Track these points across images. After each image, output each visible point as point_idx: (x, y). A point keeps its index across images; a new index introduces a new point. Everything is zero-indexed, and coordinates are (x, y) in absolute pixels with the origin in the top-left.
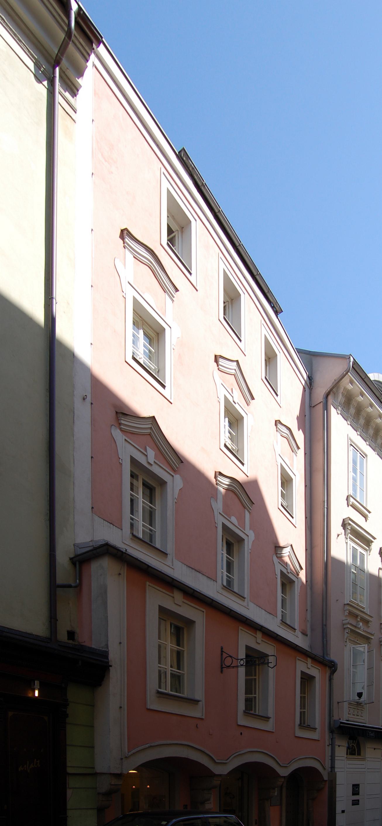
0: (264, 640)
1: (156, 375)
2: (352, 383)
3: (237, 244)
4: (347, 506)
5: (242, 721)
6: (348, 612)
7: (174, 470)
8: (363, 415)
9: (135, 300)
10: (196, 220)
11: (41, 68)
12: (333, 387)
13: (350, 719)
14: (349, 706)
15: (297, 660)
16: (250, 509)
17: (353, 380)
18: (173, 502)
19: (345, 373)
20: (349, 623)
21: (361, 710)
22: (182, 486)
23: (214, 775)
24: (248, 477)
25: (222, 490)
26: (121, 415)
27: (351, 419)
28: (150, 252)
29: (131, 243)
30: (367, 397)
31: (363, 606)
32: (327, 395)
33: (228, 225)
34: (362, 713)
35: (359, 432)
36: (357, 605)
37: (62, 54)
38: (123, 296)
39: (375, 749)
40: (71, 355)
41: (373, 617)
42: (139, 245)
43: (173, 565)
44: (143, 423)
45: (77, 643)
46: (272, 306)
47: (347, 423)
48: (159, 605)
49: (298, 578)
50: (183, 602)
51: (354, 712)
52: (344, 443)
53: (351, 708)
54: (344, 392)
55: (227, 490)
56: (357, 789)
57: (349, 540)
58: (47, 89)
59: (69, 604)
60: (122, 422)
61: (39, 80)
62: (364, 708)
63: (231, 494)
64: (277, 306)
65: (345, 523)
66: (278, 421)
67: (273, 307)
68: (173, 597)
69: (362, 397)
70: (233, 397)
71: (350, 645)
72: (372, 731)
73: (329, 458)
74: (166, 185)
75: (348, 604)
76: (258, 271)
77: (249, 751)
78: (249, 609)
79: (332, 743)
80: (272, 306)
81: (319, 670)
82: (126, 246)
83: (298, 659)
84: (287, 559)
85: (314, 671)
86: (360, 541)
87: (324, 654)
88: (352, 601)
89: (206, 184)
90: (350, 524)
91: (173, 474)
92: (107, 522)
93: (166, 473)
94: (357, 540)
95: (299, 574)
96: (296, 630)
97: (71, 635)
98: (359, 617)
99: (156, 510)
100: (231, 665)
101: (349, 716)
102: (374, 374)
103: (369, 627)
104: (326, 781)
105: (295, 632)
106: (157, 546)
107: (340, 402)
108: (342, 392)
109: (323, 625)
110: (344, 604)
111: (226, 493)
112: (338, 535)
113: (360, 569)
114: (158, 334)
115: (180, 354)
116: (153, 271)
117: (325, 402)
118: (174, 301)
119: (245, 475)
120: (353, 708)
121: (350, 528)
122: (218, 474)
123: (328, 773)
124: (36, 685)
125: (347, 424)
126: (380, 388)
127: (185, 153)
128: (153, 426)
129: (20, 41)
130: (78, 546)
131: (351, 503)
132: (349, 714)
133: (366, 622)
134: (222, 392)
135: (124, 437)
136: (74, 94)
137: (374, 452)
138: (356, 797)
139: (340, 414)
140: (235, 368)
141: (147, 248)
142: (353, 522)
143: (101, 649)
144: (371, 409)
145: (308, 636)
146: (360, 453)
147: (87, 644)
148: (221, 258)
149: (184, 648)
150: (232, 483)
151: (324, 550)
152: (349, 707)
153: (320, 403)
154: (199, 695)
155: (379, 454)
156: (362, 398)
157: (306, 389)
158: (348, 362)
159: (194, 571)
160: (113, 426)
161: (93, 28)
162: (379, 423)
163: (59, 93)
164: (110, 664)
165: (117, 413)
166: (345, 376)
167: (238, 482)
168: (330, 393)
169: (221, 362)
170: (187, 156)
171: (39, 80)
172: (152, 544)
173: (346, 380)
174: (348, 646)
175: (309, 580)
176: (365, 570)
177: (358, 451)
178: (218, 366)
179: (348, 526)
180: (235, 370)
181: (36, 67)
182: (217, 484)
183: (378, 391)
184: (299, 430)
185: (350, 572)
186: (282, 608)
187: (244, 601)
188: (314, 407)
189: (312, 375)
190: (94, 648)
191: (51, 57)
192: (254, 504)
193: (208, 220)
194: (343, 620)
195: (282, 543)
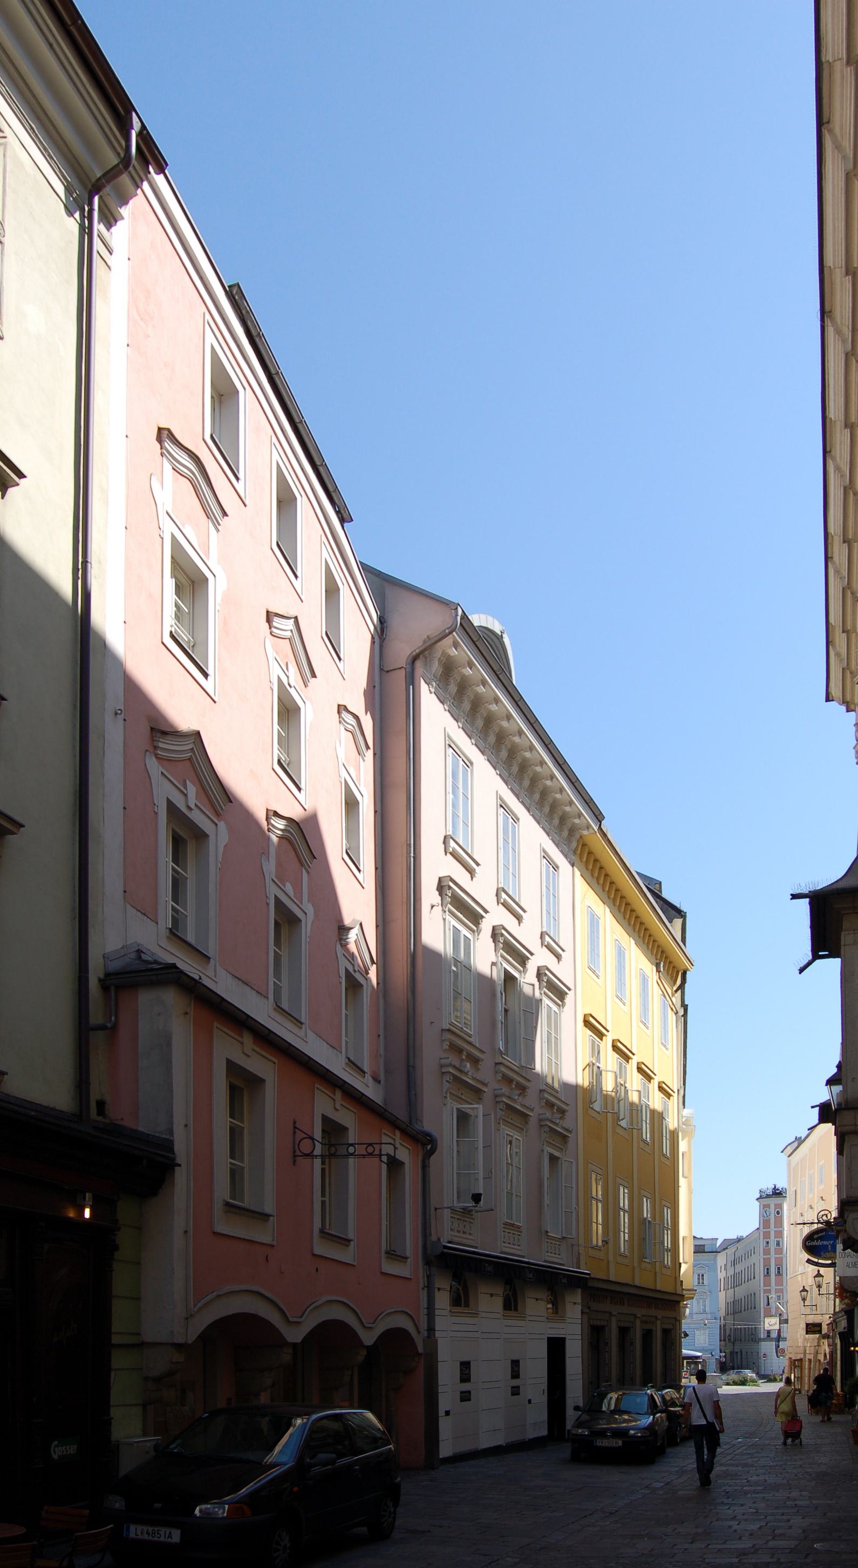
0: (345, 1104)
1: (189, 649)
2: (457, 647)
3: (297, 420)
4: (444, 853)
5: (320, 1248)
6: (501, 1075)
7: (218, 815)
8: (468, 695)
9: (174, 538)
10: (343, 584)
11: (73, 193)
12: (425, 650)
13: (455, 1239)
14: (453, 1215)
15: (383, 1134)
16: (310, 867)
17: (458, 642)
18: (216, 869)
19: (447, 631)
20: (450, 1064)
21: (470, 1222)
22: (227, 840)
23: (287, 1344)
24: (305, 810)
25: (274, 839)
26: (159, 735)
27: (450, 701)
28: (202, 471)
29: (171, 447)
30: (478, 670)
31: (469, 1032)
32: (415, 659)
33: (289, 394)
34: (470, 1227)
35: (461, 722)
36: (461, 1031)
37: (108, 182)
38: (160, 535)
39: (492, 1295)
40: (103, 644)
41: (485, 1053)
42: (182, 451)
43: (215, 976)
44: (186, 743)
45: (107, 1121)
46: (337, 510)
47: (459, 726)
48: (227, 1059)
49: (366, 979)
50: (253, 1050)
51: (459, 1227)
52: (493, 802)
53: (454, 1218)
54: (442, 658)
55: (280, 838)
56: (467, 1372)
57: (449, 918)
58: (79, 224)
59: (98, 1054)
60: (161, 745)
61: (69, 211)
62: (474, 1219)
63: (285, 843)
64: (346, 512)
65: (442, 884)
66: (343, 707)
67: (338, 513)
68: (242, 1043)
69: (471, 668)
70: (288, 677)
71: (451, 1103)
72: (490, 1263)
73: (417, 770)
74: (210, 339)
75: (449, 1030)
76: (324, 461)
77: (326, 1300)
78: (307, 1042)
79: (428, 1284)
80: (337, 510)
81: (409, 1149)
82: (164, 454)
83: (384, 1133)
84: (352, 947)
85: (403, 1154)
86: (463, 916)
87: (410, 1120)
88: (454, 1023)
89: (265, 335)
90: (450, 888)
91: (216, 821)
92: (135, 910)
93: (207, 820)
94: (459, 914)
95: (369, 971)
96: (367, 1073)
97: (101, 1105)
98: (465, 1053)
99: (187, 878)
100: (310, 1153)
101: (452, 1233)
102: (479, 616)
103: (479, 1069)
104: (421, 1354)
105: (364, 1077)
106: (188, 939)
107: (434, 674)
108: (440, 658)
109: (408, 1066)
110: (442, 1030)
111: (279, 842)
112: (432, 907)
113: (464, 966)
114: (194, 582)
115: (225, 618)
116: (195, 487)
117: (411, 671)
118: (219, 531)
119: (301, 807)
120: (458, 1219)
121: (450, 895)
122: (272, 813)
123: (424, 1340)
124: (87, 1199)
125: (457, 726)
126: (486, 637)
127: (239, 291)
128: (195, 745)
129: (51, 157)
130: (108, 958)
131: (502, 901)
132: (451, 1229)
133: (475, 1061)
134: (276, 671)
135: (161, 769)
136: (109, 226)
137: (482, 755)
138: (466, 1387)
139: (434, 693)
140: (291, 627)
141: (190, 453)
142: (455, 885)
143: (157, 1135)
144: (455, 651)
145: (382, 1082)
146: (463, 760)
147: (129, 1123)
148: (274, 445)
149: (242, 1121)
150: (289, 826)
151: (410, 933)
152: (452, 1217)
153: (400, 668)
154: (269, 1208)
155: (490, 760)
156: (470, 671)
157: (376, 640)
158: (454, 615)
159: (241, 982)
160: (148, 753)
161: (156, 152)
162: (466, 676)
163: (99, 236)
164: (176, 1162)
165: (152, 729)
166: (446, 636)
167: (294, 820)
168: (419, 656)
169: (277, 622)
170: (241, 295)
171: (69, 211)
172: (177, 933)
173: (448, 641)
174: (448, 1104)
175: (381, 982)
176: (471, 967)
177: (550, 864)
178: (270, 628)
179: (448, 891)
180: (291, 631)
181: (67, 192)
182: (269, 830)
183: (484, 644)
184: (366, 714)
185: (450, 972)
186: (346, 1037)
187: (301, 1028)
188: (388, 672)
189: (384, 614)
190: (142, 1133)
191: (88, 177)
192: (315, 858)
193: (259, 385)
194: (441, 1059)
195: (347, 921)
